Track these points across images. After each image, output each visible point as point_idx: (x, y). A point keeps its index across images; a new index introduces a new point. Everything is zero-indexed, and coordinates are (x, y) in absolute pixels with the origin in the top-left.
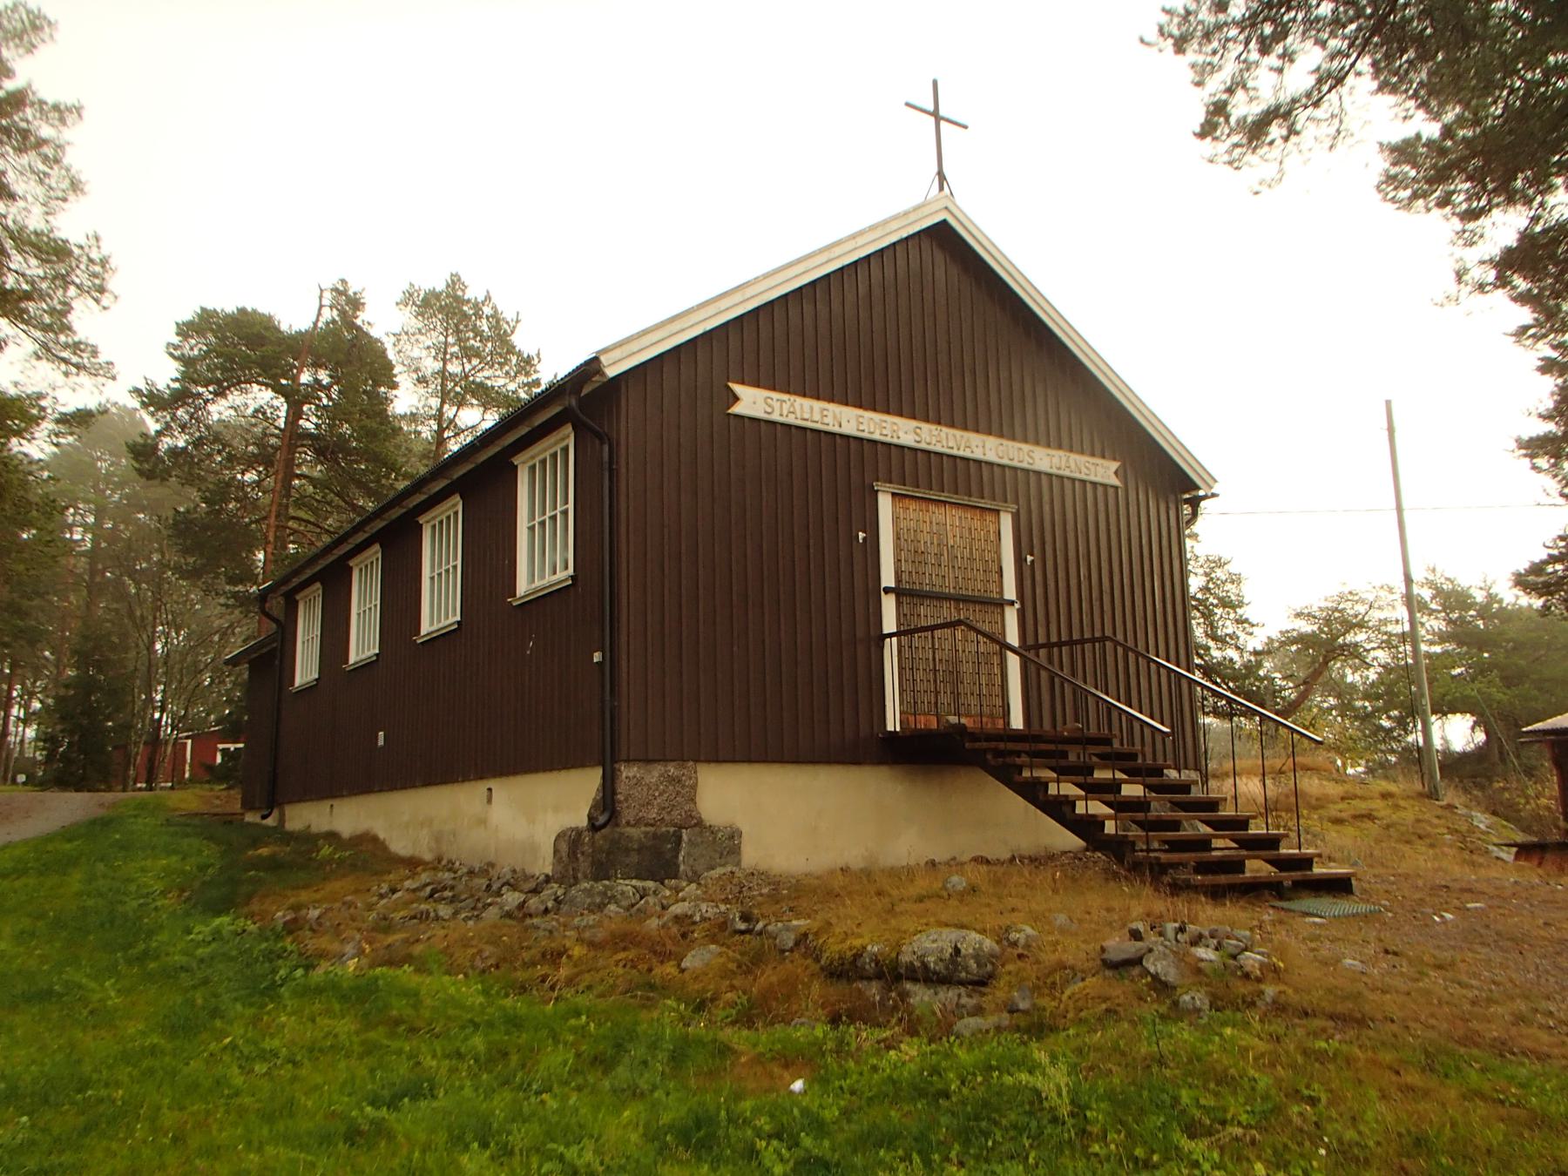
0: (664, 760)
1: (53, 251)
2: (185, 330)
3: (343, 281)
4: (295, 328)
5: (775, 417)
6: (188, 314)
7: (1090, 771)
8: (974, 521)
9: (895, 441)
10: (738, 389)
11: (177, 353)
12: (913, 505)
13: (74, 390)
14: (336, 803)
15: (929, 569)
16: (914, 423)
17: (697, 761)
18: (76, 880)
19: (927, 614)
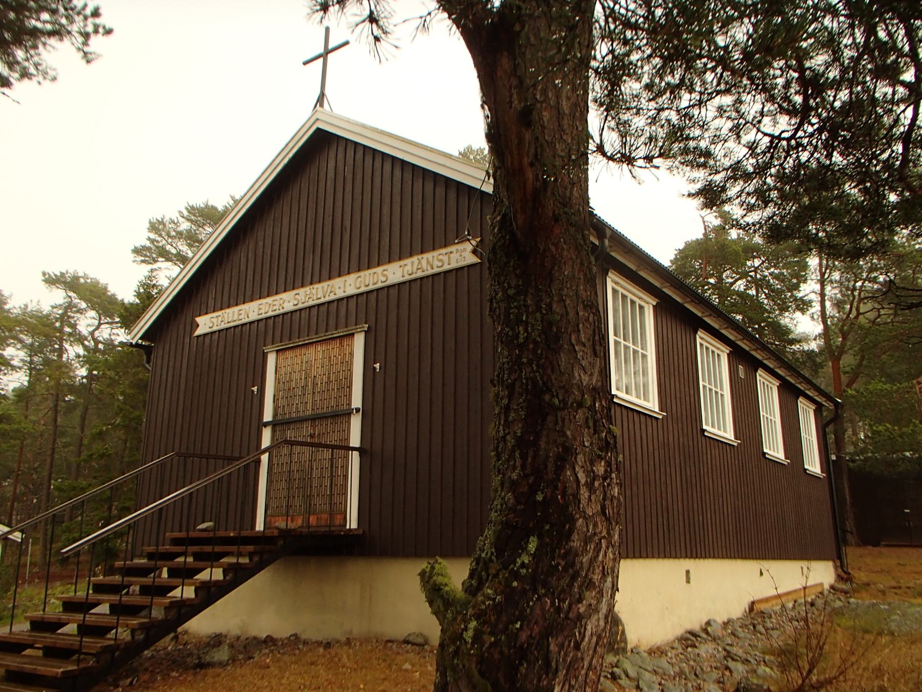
8: (334, 349)
13: (761, 574)
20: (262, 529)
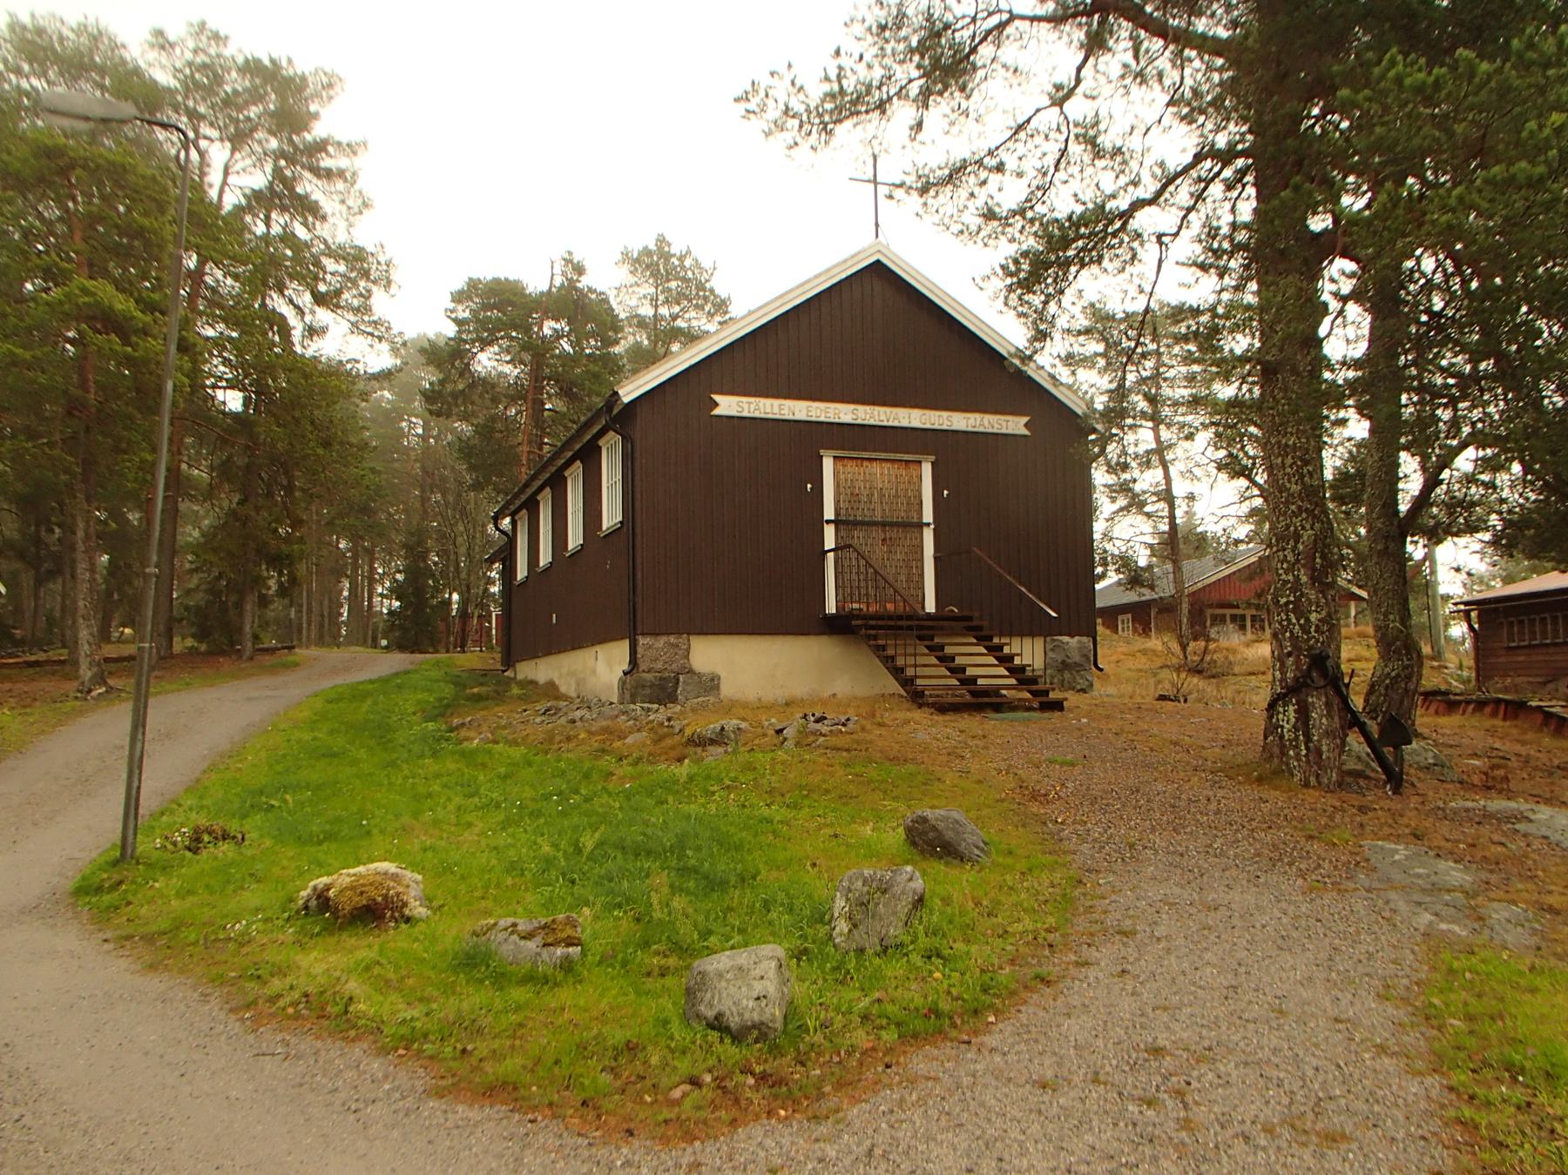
1: (356, 258)
2: (459, 297)
3: (570, 253)
4: (539, 289)
5: (745, 414)
6: (459, 284)
7: (991, 639)
9: (837, 420)
10: (717, 398)
11: (453, 316)
12: (850, 463)
14: (538, 661)
16: (851, 407)
17: (689, 634)
18: (366, 706)
19: (859, 536)
20: (834, 611)
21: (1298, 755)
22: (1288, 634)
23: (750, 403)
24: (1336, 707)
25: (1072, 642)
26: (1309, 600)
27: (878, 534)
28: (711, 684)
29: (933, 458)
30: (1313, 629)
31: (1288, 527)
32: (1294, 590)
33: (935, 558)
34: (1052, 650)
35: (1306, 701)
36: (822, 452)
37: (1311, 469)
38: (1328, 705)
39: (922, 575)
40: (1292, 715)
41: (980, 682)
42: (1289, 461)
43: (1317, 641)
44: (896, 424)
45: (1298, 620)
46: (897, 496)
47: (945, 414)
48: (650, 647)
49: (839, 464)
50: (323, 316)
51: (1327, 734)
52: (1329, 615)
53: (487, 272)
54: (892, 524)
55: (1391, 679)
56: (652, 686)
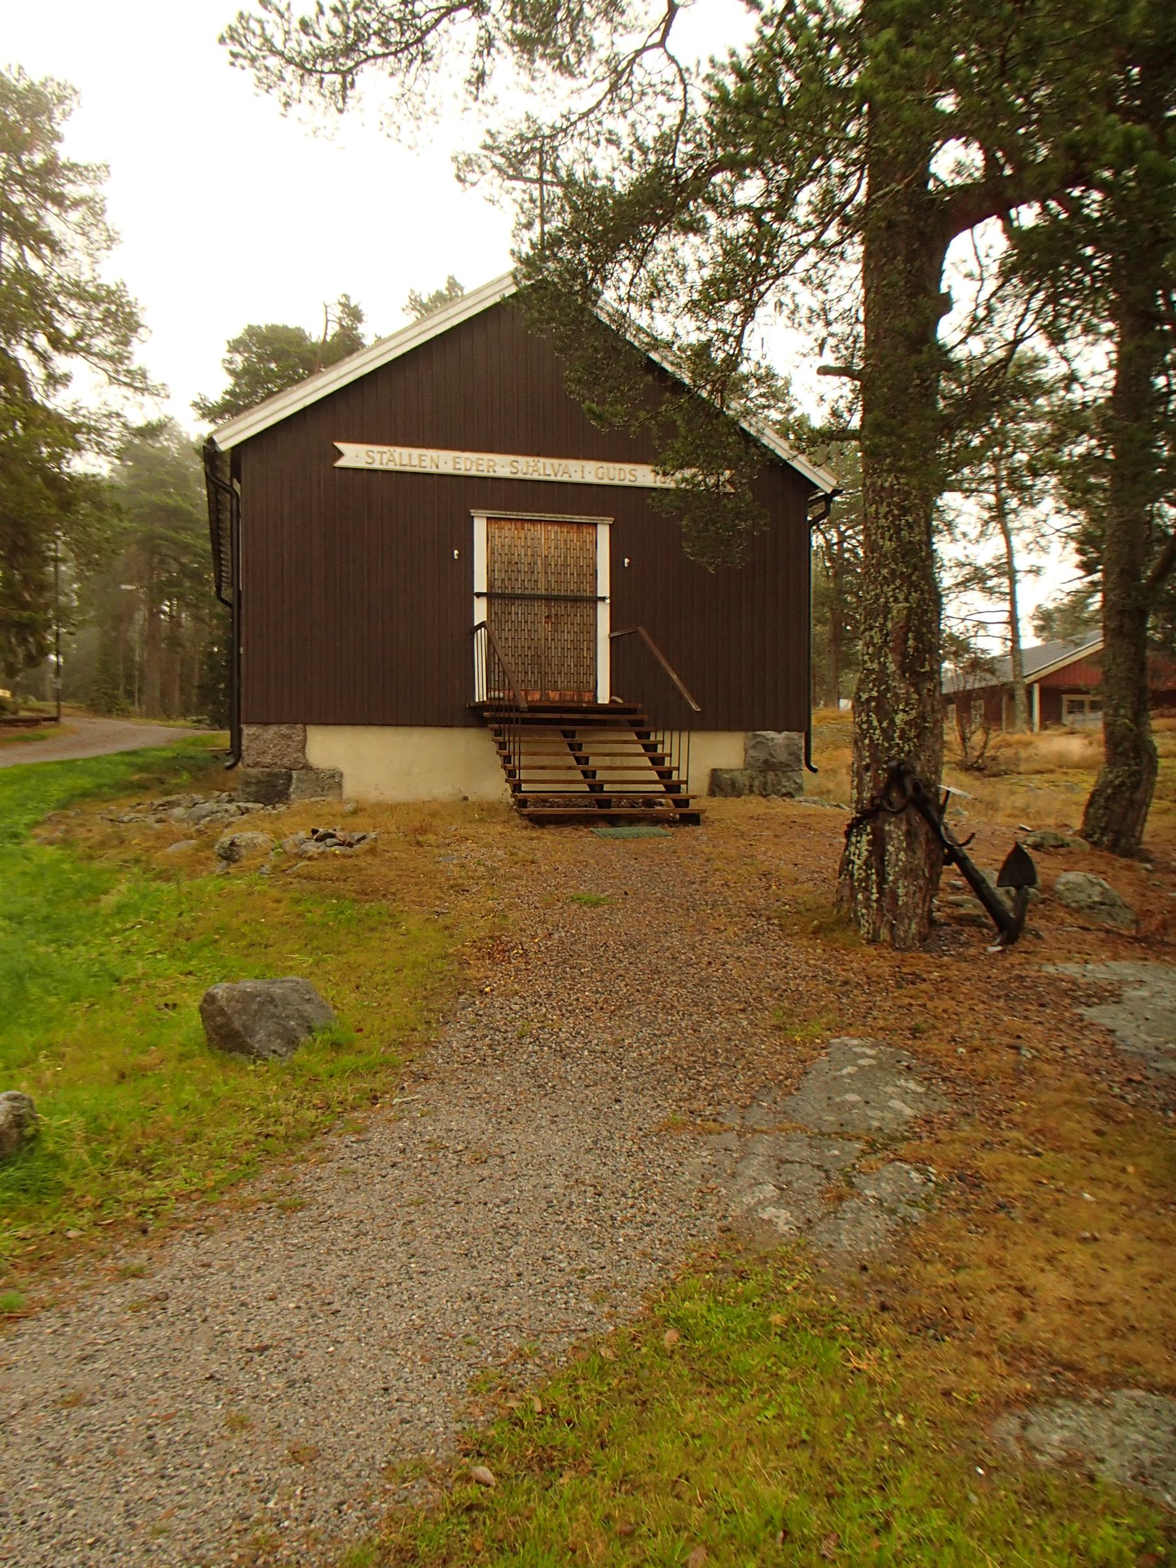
0: (280, 723)
2: (236, 346)
5: (377, 466)
6: (237, 333)
9: (491, 474)
10: (341, 446)
12: (507, 526)
15: (522, 576)
17: (305, 724)
21: (868, 899)
22: (867, 741)
23: (382, 453)
24: (922, 838)
25: (778, 738)
26: (896, 695)
27: (541, 609)
28: (332, 781)
29: (611, 520)
30: (897, 735)
31: (877, 597)
32: (878, 682)
33: (611, 639)
34: (754, 747)
35: (882, 830)
36: (473, 512)
37: (910, 519)
38: (910, 835)
39: (594, 659)
40: (864, 847)
41: (606, 788)
42: (884, 509)
43: (901, 750)
44: (566, 478)
45: (880, 722)
46: (565, 565)
47: (627, 467)
48: (257, 738)
49: (494, 526)
50: (62, 363)
51: (909, 873)
52: (922, 717)
53: (264, 319)
54: (557, 599)
55: (1114, 788)
56: (259, 782)
